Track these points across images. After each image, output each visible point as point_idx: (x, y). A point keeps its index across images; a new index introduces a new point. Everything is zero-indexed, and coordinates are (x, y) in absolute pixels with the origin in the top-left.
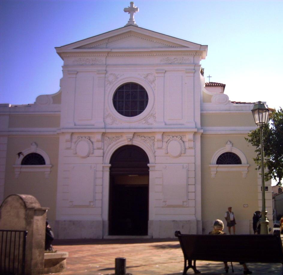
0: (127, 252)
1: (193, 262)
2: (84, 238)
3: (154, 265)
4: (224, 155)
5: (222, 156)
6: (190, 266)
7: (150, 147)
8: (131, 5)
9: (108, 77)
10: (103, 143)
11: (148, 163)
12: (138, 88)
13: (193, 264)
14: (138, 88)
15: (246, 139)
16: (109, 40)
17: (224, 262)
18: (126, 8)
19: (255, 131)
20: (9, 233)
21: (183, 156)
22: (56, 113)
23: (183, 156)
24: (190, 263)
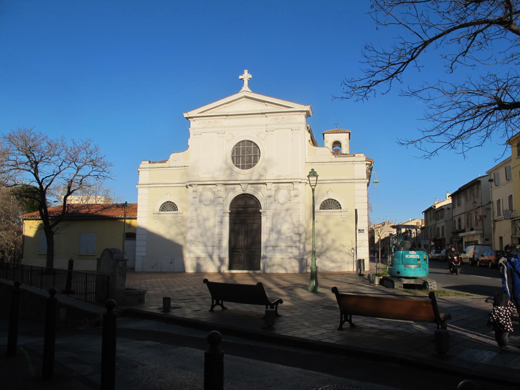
0: (356, 259)
1: (349, 316)
2: (46, 264)
3: (404, 279)
4: (330, 200)
5: (327, 201)
6: (346, 320)
7: (476, 218)
8: (221, 307)
9: (279, 232)
10: (504, 219)
11: (244, 84)
12: (437, 250)
13: (349, 318)
14: (437, 250)
15: (399, 95)
16: (472, 127)
17: (266, 306)
18: (189, 147)
19: (108, 216)
20: (74, 272)
21: (391, 74)
22: (320, 329)
23: (391, 74)
24: (346, 318)
